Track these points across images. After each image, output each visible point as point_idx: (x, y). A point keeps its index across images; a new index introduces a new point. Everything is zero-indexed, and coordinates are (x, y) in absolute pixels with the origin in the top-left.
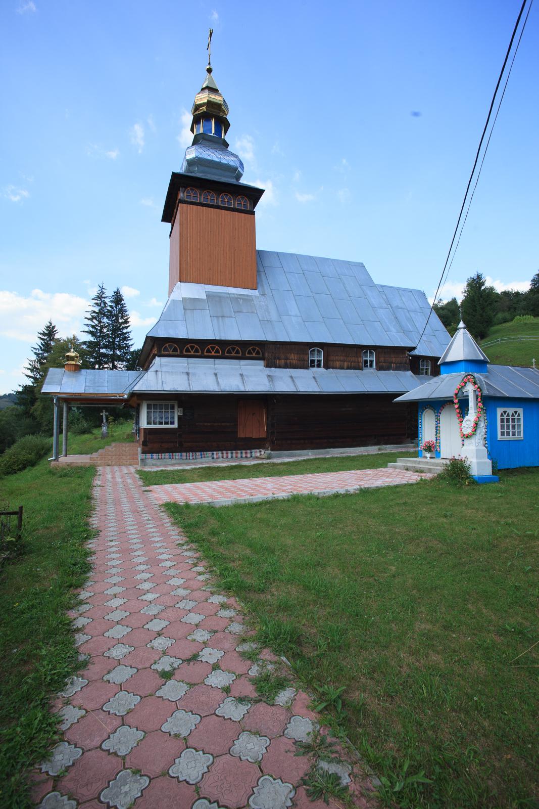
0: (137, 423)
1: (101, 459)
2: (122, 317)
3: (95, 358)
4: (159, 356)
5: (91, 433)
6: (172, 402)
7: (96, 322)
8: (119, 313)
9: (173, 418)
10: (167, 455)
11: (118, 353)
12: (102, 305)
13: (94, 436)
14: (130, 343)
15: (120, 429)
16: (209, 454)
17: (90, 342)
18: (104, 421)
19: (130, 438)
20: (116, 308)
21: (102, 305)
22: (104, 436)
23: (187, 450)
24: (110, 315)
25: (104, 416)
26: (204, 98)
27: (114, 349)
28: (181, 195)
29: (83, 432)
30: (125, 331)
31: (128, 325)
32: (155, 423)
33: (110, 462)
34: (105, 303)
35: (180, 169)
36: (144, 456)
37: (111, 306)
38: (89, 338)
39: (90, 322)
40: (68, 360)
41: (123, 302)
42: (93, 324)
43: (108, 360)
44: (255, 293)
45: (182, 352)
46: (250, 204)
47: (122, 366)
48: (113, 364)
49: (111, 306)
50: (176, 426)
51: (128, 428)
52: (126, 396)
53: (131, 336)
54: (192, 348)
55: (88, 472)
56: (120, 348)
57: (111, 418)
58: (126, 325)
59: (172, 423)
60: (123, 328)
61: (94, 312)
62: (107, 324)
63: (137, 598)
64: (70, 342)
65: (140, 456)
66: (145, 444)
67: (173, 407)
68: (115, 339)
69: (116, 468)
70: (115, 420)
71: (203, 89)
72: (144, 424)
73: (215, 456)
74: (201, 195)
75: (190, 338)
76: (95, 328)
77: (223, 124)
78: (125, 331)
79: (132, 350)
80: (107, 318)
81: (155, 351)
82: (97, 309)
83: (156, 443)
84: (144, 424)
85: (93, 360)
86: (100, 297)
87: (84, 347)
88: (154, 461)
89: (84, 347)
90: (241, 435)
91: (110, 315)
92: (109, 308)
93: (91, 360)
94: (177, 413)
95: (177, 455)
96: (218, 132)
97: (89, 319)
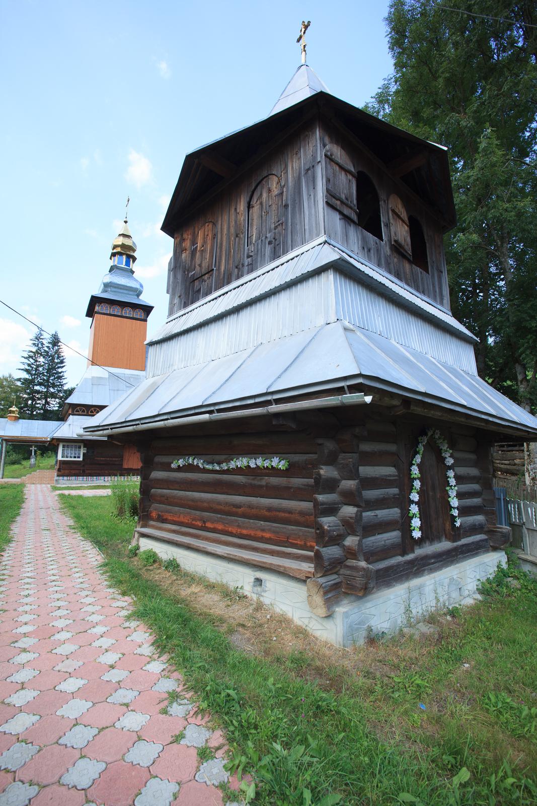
0: (57, 456)
1: (29, 480)
2: (58, 358)
3: (29, 394)
4: (72, 415)
5: (20, 464)
6: (79, 444)
7: (32, 361)
8: (56, 353)
9: (79, 454)
10: (73, 478)
11: (52, 390)
12: (40, 346)
13: (23, 466)
14: (64, 381)
15: (46, 461)
16: (102, 478)
17: (26, 380)
18: (33, 454)
19: (52, 467)
20: (53, 349)
21: (40, 346)
22: (31, 467)
23: (88, 475)
24: (46, 355)
25: (33, 451)
26: (120, 241)
27: (48, 387)
28: (97, 308)
29: (14, 463)
30: (60, 370)
31: (63, 365)
32: (67, 457)
33: (34, 482)
34: (42, 344)
35: (97, 292)
36: (58, 478)
37: (48, 347)
38: (25, 375)
39: (26, 361)
40: (10, 413)
41: (60, 344)
42: (29, 362)
43: (41, 396)
44: (143, 373)
45: (88, 412)
46: (145, 314)
47: (54, 403)
48: (46, 401)
49: (48, 347)
50: (81, 459)
51: (52, 461)
52: (49, 439)
53: (66, 375)
54: (95, 410)
55: (23, 485)
56: (54, 386)
57: (39, 452)
58: (61, 365)
59: (79, 457)
60: (58, 368)
61: (31, 352)
62: (43, 364)
63: (53, 669)
64: (5, 379)
65: (56, 478)
66: (59, 470)
67: (80, 447)
68: (49, 377)
69: (38, 486)
70: (42, 455)
71: (120, 235)
72: (60, 458)
73: (106, 480)
74: (110, 308)
75: (93, 404)
76: (31, 367)
77: (131, 258)
78: (60, 370)
79: (65, 388)
80: (44, 357)
81: (70, 412)
82: (34, 349)
83: (67, 469)
84: (60, 458)
85: (27, 396)
86: (38, 338)
87: (19, 384)
88: (64, 482)
89: (19, 384)
90: (125, 466)
91: (46, 355)
92: (46, 349)
93: (25, 396)
94: (83, 451)
95: (81, 478)
96: (128, 264)
97: (25, 358)
